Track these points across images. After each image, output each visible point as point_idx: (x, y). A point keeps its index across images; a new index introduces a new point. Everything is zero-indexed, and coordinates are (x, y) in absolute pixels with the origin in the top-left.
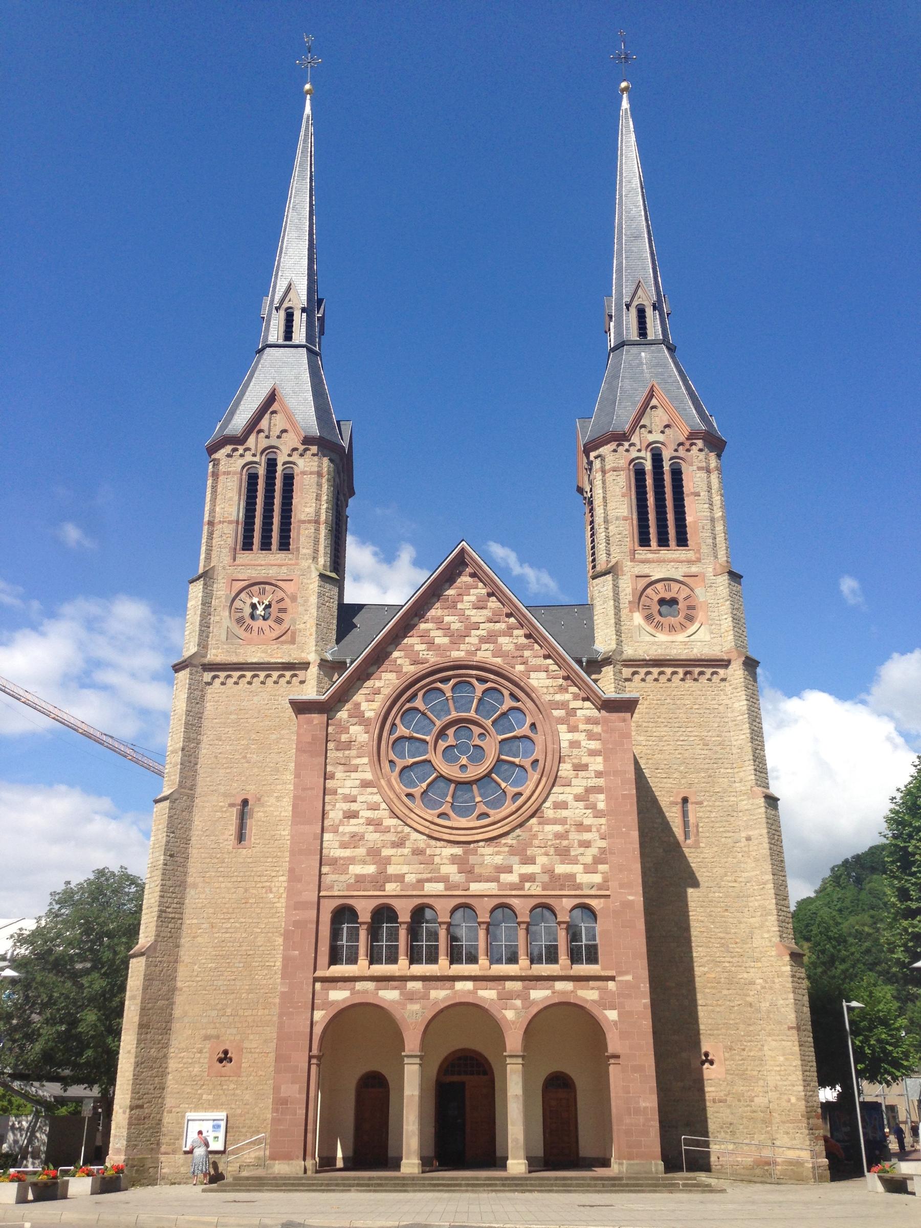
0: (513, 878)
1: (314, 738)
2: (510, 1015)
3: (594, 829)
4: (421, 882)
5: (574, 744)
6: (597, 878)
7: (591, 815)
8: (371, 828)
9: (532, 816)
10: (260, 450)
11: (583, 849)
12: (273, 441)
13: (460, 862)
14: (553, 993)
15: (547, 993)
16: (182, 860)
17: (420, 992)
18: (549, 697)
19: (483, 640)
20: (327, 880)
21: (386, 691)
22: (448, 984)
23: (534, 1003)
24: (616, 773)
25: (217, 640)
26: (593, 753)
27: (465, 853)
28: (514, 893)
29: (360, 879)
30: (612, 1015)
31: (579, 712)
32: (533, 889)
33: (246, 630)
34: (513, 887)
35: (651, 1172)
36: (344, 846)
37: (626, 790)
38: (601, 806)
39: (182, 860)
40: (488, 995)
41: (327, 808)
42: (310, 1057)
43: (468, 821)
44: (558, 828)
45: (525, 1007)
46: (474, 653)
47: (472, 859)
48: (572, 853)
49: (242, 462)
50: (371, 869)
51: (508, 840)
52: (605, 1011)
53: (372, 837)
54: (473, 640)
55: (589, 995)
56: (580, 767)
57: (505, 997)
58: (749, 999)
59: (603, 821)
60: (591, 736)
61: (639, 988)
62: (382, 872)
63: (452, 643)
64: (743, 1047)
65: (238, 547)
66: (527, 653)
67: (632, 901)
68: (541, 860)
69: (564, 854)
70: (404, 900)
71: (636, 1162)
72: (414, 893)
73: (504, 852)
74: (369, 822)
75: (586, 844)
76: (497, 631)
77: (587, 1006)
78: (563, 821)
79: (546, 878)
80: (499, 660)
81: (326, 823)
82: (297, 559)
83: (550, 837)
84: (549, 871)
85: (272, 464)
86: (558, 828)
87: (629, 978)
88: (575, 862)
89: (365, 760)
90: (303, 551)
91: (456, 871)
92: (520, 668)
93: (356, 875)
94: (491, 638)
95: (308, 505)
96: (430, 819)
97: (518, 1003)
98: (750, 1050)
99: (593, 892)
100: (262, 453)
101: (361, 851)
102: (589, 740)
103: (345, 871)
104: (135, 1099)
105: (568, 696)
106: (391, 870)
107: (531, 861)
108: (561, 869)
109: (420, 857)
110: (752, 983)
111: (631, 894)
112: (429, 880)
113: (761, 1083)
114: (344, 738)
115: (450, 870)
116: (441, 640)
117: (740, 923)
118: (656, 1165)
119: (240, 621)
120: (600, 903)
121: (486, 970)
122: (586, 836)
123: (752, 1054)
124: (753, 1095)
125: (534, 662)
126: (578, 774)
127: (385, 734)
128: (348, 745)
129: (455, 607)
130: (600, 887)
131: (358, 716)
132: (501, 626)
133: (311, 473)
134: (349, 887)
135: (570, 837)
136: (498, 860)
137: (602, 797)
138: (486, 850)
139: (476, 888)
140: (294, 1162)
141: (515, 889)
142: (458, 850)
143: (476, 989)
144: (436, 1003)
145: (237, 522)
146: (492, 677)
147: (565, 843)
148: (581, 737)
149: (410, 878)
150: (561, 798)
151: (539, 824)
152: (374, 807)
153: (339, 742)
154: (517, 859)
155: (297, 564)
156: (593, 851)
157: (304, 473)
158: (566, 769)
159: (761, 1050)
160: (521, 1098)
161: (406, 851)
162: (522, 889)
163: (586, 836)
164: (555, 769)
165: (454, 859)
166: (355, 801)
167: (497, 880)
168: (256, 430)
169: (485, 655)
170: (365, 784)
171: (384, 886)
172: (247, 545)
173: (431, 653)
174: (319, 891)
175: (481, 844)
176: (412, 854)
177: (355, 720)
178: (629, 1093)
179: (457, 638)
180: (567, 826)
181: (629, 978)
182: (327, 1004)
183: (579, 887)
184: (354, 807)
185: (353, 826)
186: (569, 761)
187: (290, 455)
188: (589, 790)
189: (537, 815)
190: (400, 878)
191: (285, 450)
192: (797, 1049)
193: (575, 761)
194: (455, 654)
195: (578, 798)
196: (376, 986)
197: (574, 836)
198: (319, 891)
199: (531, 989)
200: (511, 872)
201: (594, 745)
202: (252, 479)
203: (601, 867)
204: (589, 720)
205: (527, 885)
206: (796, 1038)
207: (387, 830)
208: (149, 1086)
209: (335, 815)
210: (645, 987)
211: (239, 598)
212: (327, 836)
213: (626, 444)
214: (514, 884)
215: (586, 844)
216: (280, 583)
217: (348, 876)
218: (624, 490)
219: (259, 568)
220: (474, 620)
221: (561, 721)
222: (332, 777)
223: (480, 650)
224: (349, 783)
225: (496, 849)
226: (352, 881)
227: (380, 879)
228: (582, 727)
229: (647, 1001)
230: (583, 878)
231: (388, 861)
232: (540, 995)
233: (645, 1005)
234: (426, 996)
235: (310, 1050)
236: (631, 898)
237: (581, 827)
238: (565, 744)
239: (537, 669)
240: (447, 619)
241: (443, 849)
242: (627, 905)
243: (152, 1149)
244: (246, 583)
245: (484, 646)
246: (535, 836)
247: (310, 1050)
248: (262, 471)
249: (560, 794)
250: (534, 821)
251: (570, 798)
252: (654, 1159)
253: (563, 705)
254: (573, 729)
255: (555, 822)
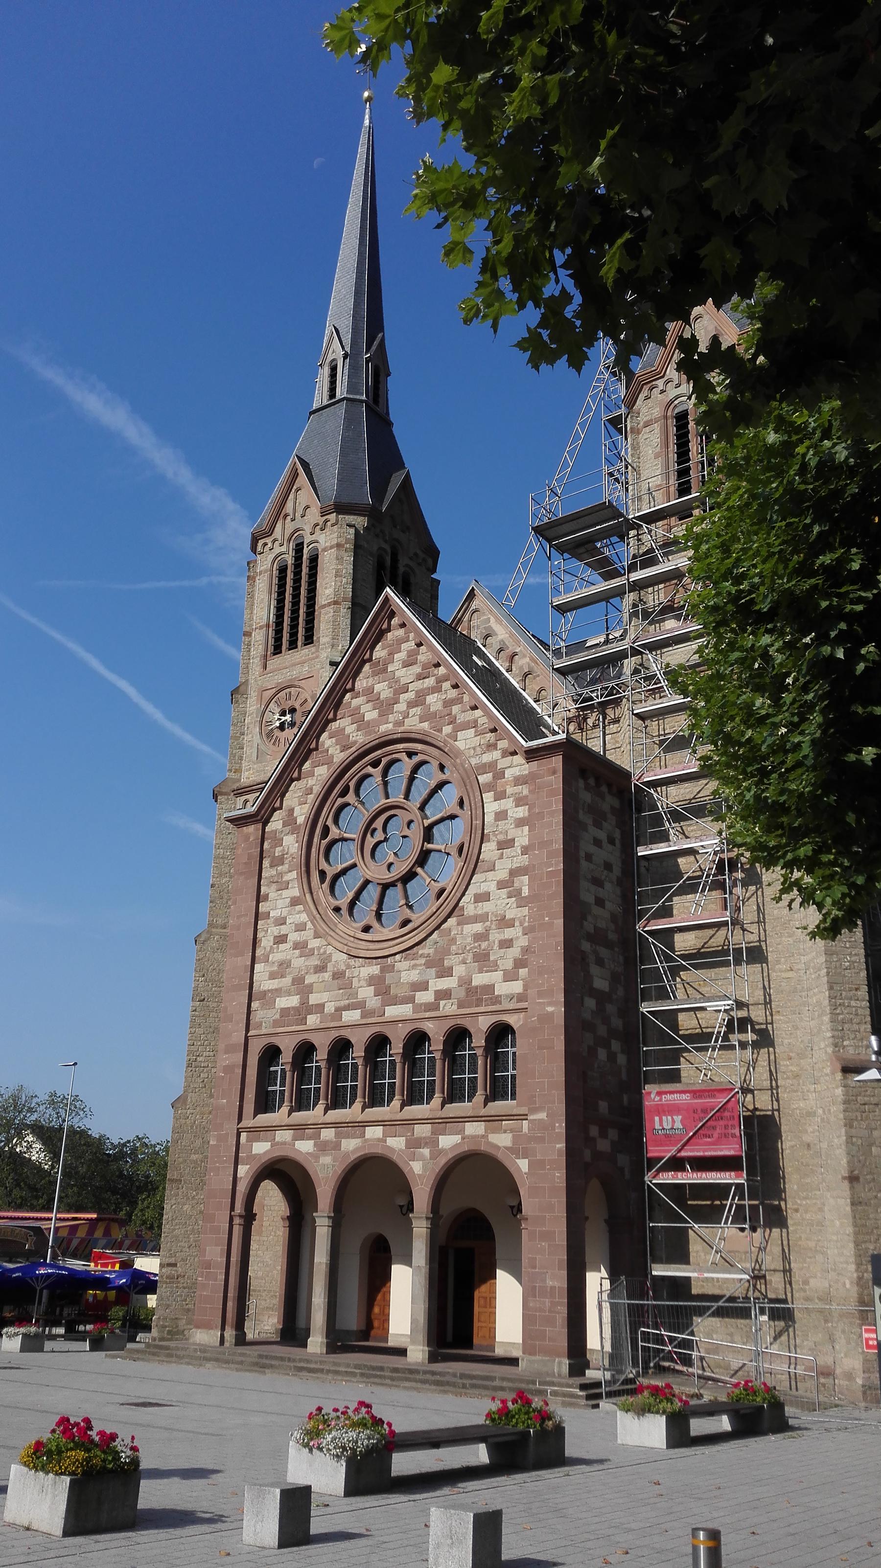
0: (425, 997)
1: (250, 856)
2: (417, 1167)
3: (517, 924)
4: (339, 1010)
5: (501, 815)
6: (516, 987)
7: (515, 905)
8: (297, 952)
9: (449, 916)
10: (286, 537)
11: (503, 950)
12: (298, 523)
13: (380, 985)
14: (463, 1138)
15: (456, 1139)
16: (215, 1005)
17: (332, 1142)
18: (474, 761)
19: (411, 704)
20: (256, 1018)
21: (317, 789)
22: (358, 1131)
23: (442, 1152)
24: (543, 844)
25: (249, 761)
26: (520, 823)
27: (383, 970)
28: (427, 1015)
29: (285, 1012)
30: (523, 1165)
31: (508, 773)
32: (448, 1007)
33: (274, 744)
34: (430, 1007)
35: (553, 1375)
36: (273, 976)
37: (552, 866)
38: (525, 892)
39: (215, 1005)
40: (397, 1143)
41: (259, 935)
42: (231, 1219)
43: (391, 931)
44: (478, 928)
45: (433, 1156)
46: (402, 723)
47: (389, 978)
48: (492, 958)
49: (271, 557)
50: (293, 1001)
51: (423, 950)
52: (517, 1161)
53: (298, 963)
54: (401, 707)
55: (502, 1140)
56: (505, 844)
57: (414, 1144)
58: (807, 1138)
59: (525, 911)
60: (520, 801)
61: (554, 1128)
62: (304, 1002)
63: (380, 715)
64: (796, 1207)
65: (269, 653)
66: (455, 709)
67: (552, 1013)
68: (459, 970)
69: (483, 960)
70: (322, 1034)
71: (537, 1358)
72: (332, 1024)
73: (421, 965)
74: (296, 946)
75: (507, 944)
76: (426, 689)
77: (395, 1158)
78: (482, 918)
79: (462, 994)
80: (425, 725)
81: (259, 952)
82: (317, 651)
83: (469, 940)
84: (466, 982)
85: (299, 549)
86: (478, 928)
87: (542, 1116)
88: (494, 967)
89: (294, 874)
90: (323, 640)
91: (372, 994)
92: (447, 729)
93: (282, 1009)
94: (419, 700)
95: (328, 586)
96: (352, 934)
97: (426, 1152)
98: (806, 1212)
99: (511, 1006)
100: (289, 540)
101: (287, 981)
102: (517, 806)
103: (272, 1004)
104: (166, 1257)
105: (496, 754)
106: (314, 999)
107: (446, 972)
108: (479, 979)
109: (339, 981)
110: (811, 1114)
111: (550, 1004)
112: (347, 1008)
113: (820, 1258)
114: (278, 851)
115: (366, 993)
116: (371, 715)
117: (797, 1028)
118: (560, 1363)
119: (270, 735)
120: (519, 1018)
121: (396, 1113)
122: (509, 933)
123: (808, 1216)
124: (808, 1275)
125: (461, 718)
126: (502, 854)
127: (316, 840)
128: (280, 861)
129: (385, 670)
130: (521, 998)
131: (290, 821)
132: (430, 682)
133: (331, 547)
134: (276, 1023)
135: (491, 938)
136: (414, 976)
137: (526, 879)
138: (401, 964)
139: (392, 1012)
140: (212, 1332)
141: (429, 1010)
142: (374, 969)
143: (295, 1139)
144: (347, 1154)
145: (268, 626)
146: (379, 752)
147: (484, 945)
148: (507, 804)
149: (330, 1008)
150: (484, 888)
151: (458, 924)
152: (300, 928)
153: (274, 857)
154: (433, 971)
155: (317, 657)
156: (515, 952)
157: (325, 550)
158: (489, 850)
159: (821, 1210)
160: (423, 1270)
161: (327, 976)
162: (437, 1008)
163: (509, 933)
164: (476, 851)
165: (372, 981)
166: (285, 923)
167: (411, 1000)
168: (282, 516)
169: (414, 724)
170: (294, 902)
171: (306, 1018)
172: (277, 650)
173: (359, 733)
174: (247, 1029)
175: (398, 957)
176: (333, 979)
177: (288, 828)
178: (535, 1267)
179: (385, 707)
180: (488, 923)
181: (542, 1116)
182: (252, 1158)
183: (497, 1000)
184: (284, 930)
185: (283, 952)
186: (494, 838)
187: (312, 534)
188: (514, 873)
189: (455, 914)
190: (320, 1007)
191: (308, 529)
192: (848, 1209)
193: (501, 837)
194: (383, 728)
195: (501, 885)
196: (294, 1135)
197: (496, 936)
198: (247, 1029)
199: (440, 1134)
200: (427, 989)
201: (522, 812)
202: (283, 570)
203: (523, 972)
204: (519, 781)
205: (442, 1003)
206: (848, 1193)
207: (312, 953)
208: (182, 1244)
209: (266, 942)
210: (560, 1127)
211: (268, 709)
212: (257, 967)
213: (660, 383)
214: (429, 1003)
215: (507, 944)
216: (296, 683)
217: (274, 1011)
218: (658, 449)
219: (285, 671)
220: (403, 681)
221: (490, 787)
222: (266, 897)
223: (408, 717)
224: (280, 904)
225: (413, 962)
226: (278, 1016)
227: (304, 1010)
228: (509, 790)
229: (561, 1146)
230: (503, 989)
231: (310, 989)
232: (448, 1142)
233: (559, 1150)
234: (337, 1146)
235: (232, 1208)
236: (550, 1009)
237: (504, 923)
238: (489, 818)
239: (465, 726)
240: (378, 688)
241: (362, 969)
242: (546, 1018)
243: (189, 1310)
244: (274, 690)
245: (412, 711)
246: (453, 941)
247: (232, 1208)
248: (290, 560)
249: (482, 883)
250: (452, 921)
251: (492, 887)
252: (559, 1356)
253: (491, 767)
254: (500, 796)
255: (476, 919)
